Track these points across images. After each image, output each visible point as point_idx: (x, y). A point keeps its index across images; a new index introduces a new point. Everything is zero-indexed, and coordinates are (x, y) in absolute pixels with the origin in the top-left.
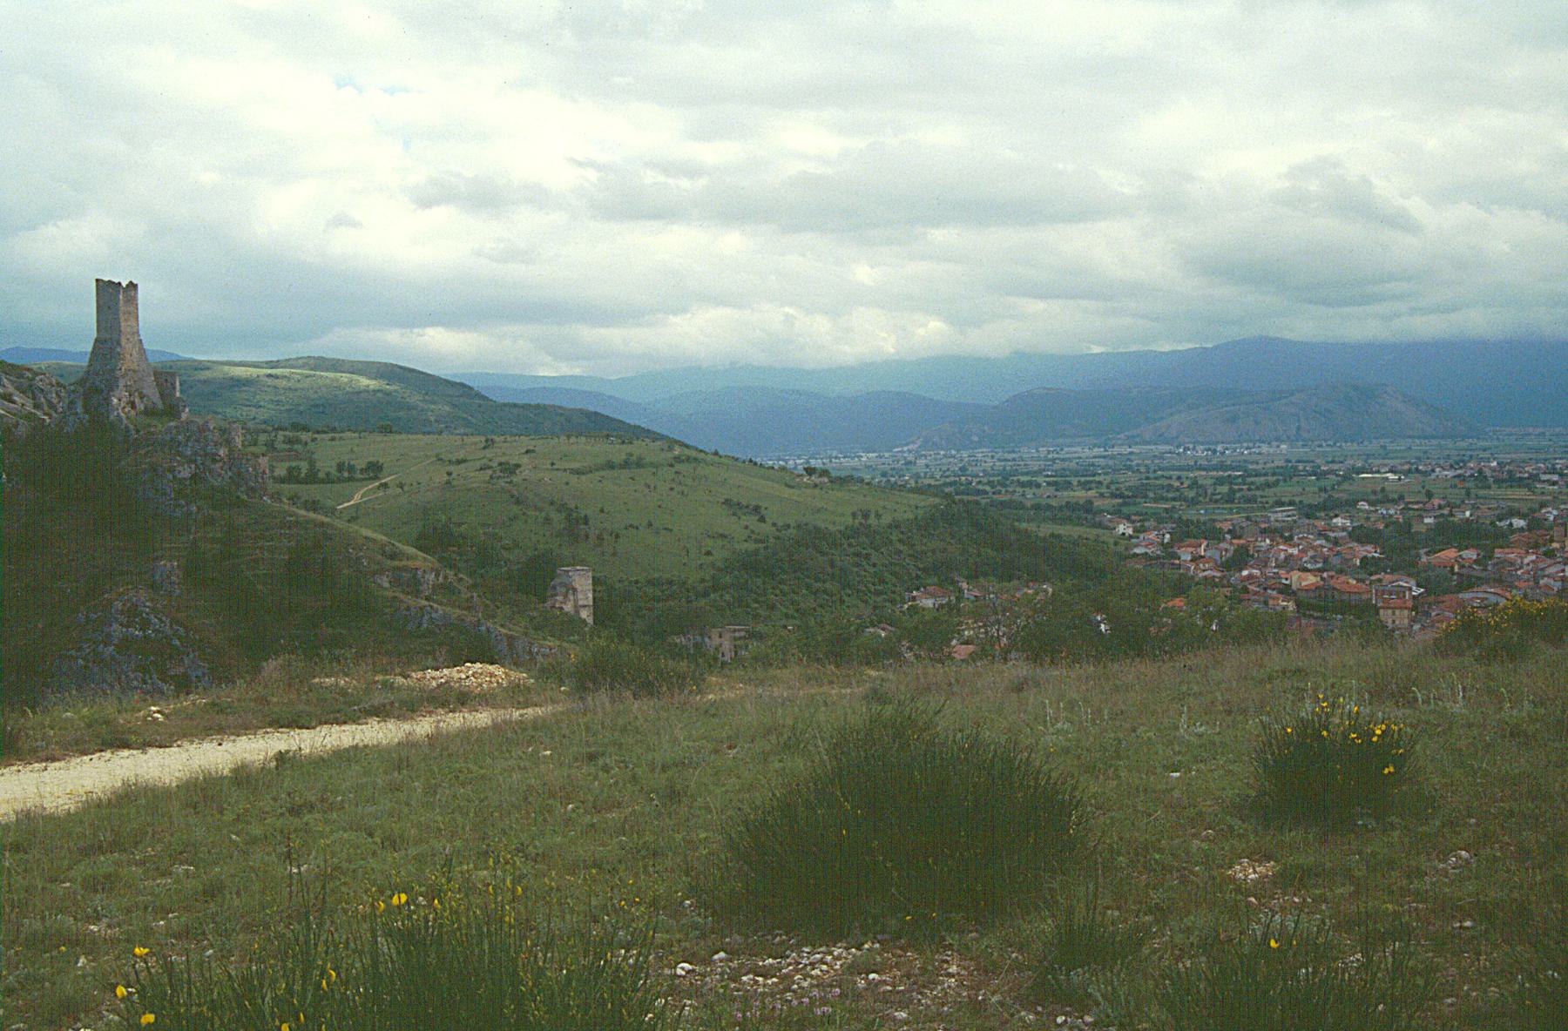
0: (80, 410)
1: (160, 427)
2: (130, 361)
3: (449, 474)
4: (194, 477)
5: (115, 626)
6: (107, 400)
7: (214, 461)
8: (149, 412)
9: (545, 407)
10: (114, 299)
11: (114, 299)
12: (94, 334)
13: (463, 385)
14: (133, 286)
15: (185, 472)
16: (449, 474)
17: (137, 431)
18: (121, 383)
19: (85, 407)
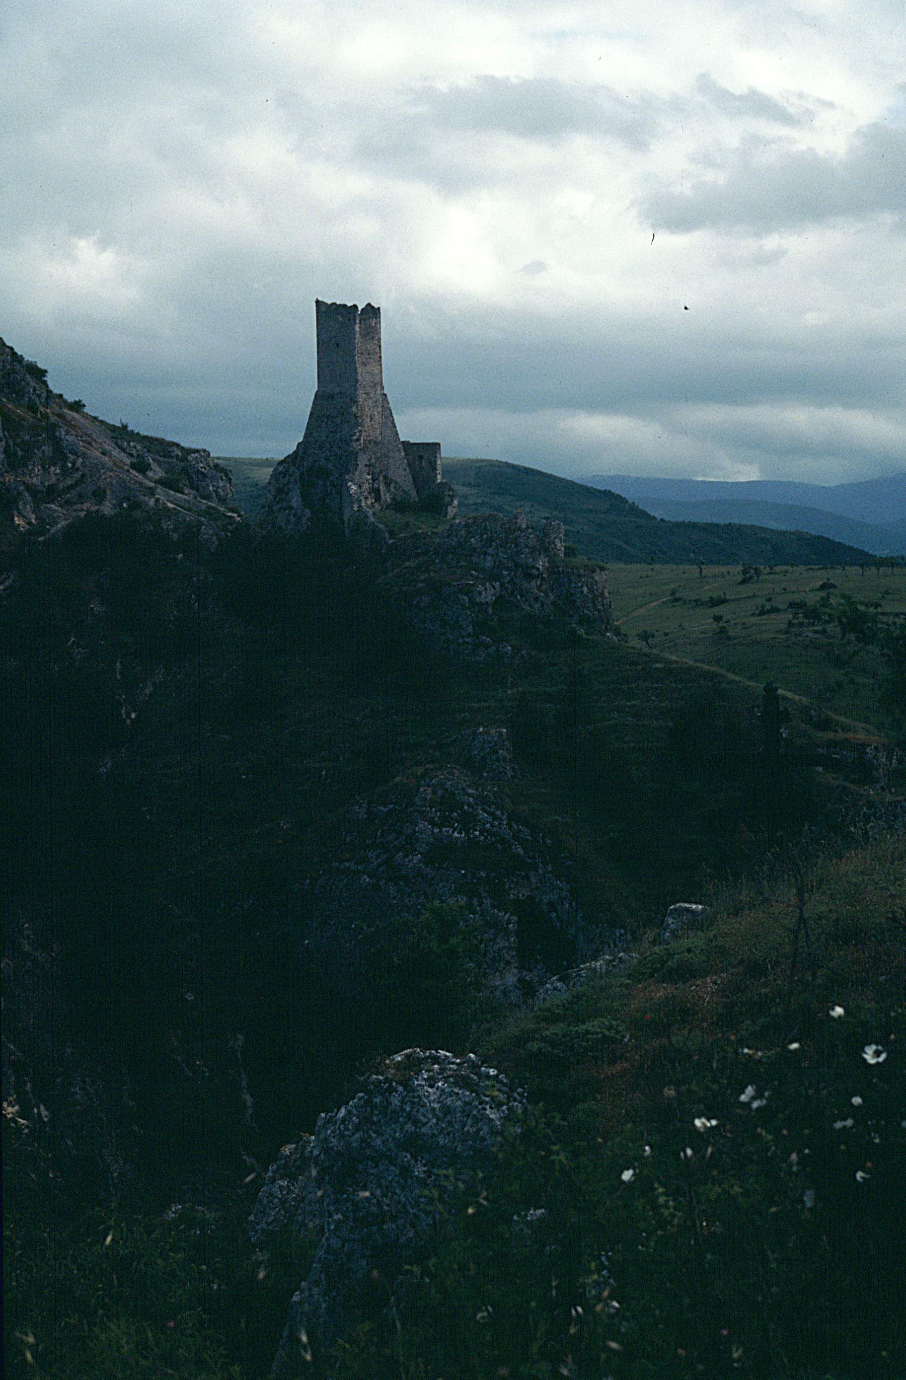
0: (296, 501)
1: (423, 525)
2: (370, 429)
3: (717, 619)
4: (500, 601)
5: (422, 825)
6: (341, 489)
7: (529, 577)
8: (400, 506)
9: (740, 527)
10: (346, 331)
11: (346, 331)
12: (312, 386)
13: (608, 494)
14: (379, 308)
15: (488, 594)
16: (717, 619)
17: (392, 534)
18: (363, 460)
19: (304, 497)
